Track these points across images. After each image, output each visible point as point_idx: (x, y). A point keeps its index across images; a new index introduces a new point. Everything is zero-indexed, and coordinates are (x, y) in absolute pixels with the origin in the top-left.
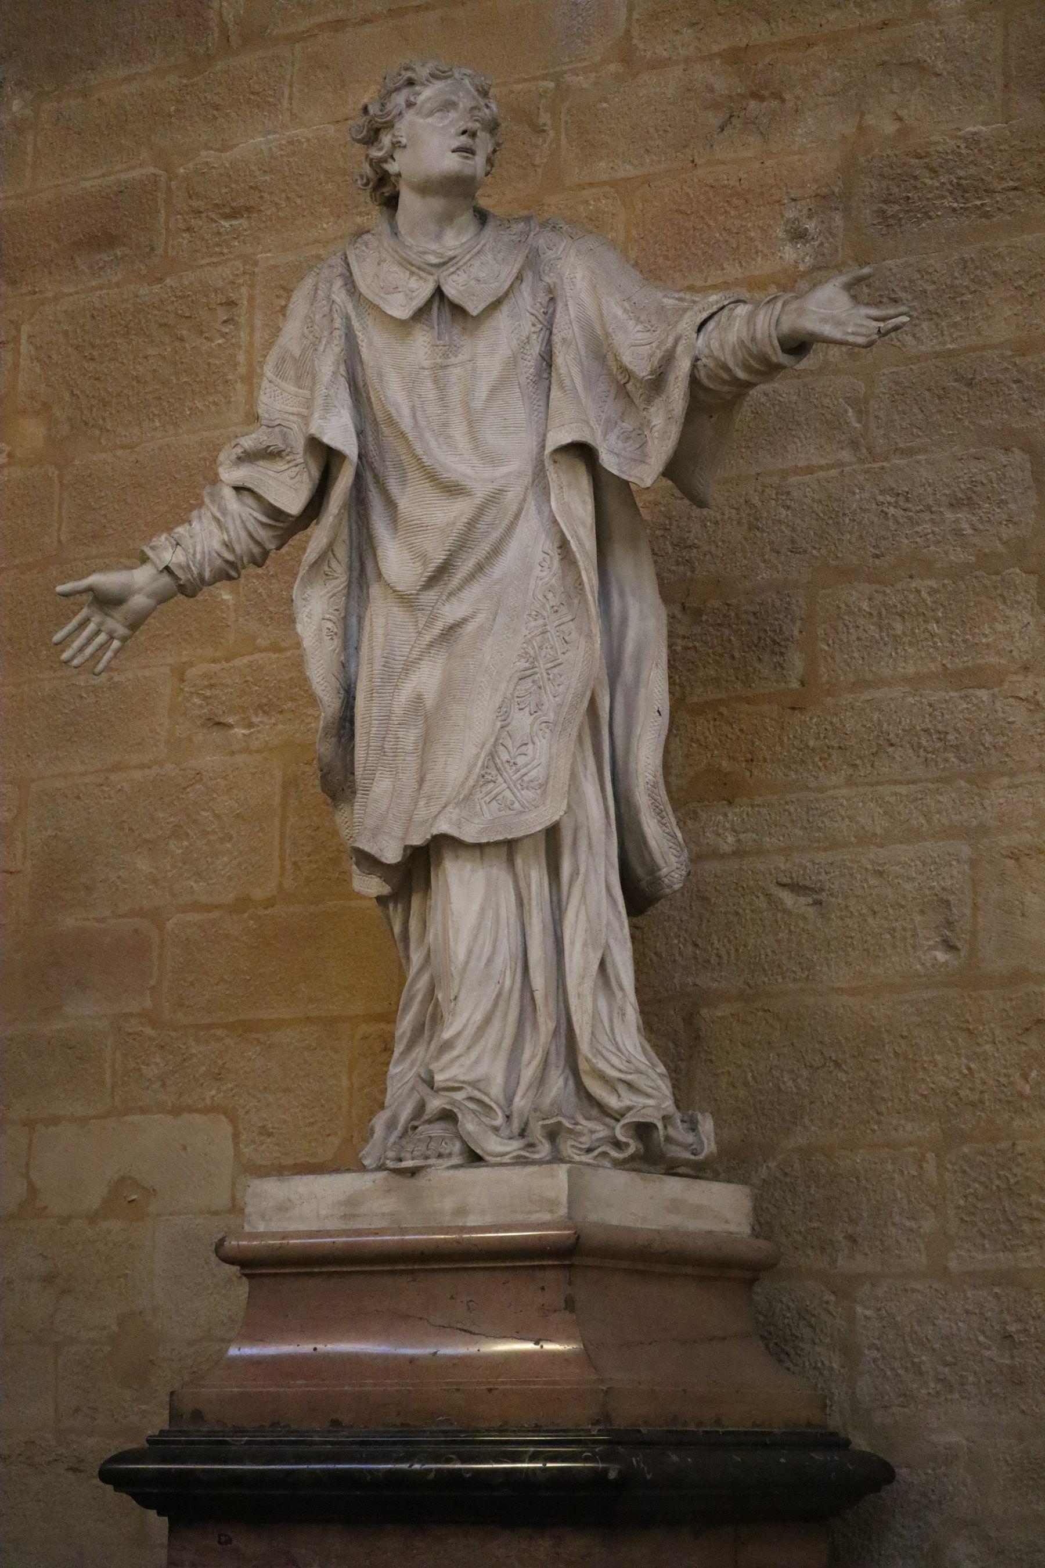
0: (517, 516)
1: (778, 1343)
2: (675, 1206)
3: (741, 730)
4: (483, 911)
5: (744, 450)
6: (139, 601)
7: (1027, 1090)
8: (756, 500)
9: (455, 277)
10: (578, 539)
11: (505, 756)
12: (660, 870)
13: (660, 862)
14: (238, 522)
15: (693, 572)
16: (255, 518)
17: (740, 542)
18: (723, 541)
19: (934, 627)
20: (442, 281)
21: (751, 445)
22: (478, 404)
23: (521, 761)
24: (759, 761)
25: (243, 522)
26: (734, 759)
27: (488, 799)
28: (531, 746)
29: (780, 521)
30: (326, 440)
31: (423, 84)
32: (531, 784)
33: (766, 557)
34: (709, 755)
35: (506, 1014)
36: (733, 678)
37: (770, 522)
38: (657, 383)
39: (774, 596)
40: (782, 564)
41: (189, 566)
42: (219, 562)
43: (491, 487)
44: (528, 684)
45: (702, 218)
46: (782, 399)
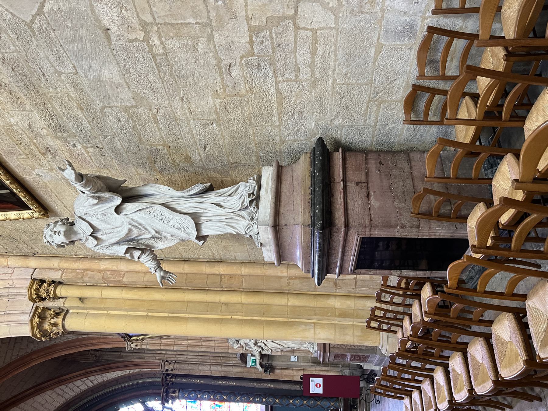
0: (132, 220)
1: (295, 157)
2: (266, 191)
4: (211, 229)
6: (162, 274)
7: (240, 111)
19: (147, 125)
23: (180, 222)
35: (230, 223)
38: (98, 198)
43: (128, 225)
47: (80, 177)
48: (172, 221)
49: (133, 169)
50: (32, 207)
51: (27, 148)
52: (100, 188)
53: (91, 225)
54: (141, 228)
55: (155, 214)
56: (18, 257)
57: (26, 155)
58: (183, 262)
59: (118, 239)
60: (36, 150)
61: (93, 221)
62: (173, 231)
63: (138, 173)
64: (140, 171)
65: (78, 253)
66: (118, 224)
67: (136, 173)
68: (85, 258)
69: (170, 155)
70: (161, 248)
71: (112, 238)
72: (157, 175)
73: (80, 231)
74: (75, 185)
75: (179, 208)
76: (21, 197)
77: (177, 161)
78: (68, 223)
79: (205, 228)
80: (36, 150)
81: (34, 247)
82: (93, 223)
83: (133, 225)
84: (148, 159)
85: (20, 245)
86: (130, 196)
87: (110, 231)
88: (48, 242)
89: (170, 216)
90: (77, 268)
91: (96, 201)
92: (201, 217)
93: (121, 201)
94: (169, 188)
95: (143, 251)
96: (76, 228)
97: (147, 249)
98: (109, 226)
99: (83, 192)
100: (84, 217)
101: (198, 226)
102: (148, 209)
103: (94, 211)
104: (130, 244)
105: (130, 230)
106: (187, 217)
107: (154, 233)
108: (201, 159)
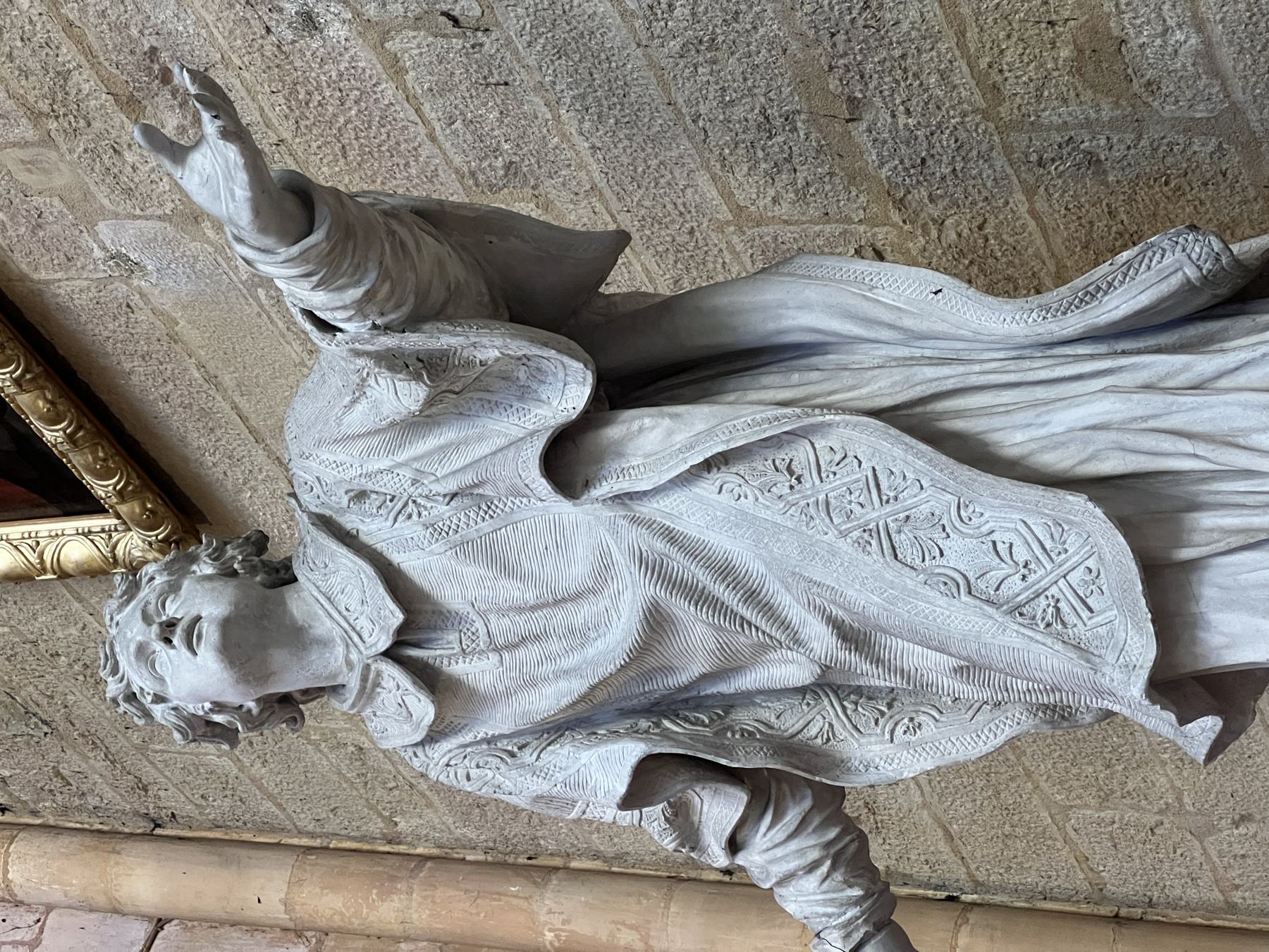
0: (671, 536)
3: (1009, 36)
5: (614, 65)
8: (675, 45)
9: (365, 636)
10: (690, 447)
11: (1015, 584)
12: (1188, 280)
13: (1175, 281)
14: (779, 852)
15: (799, 112)
16: (769, 828)
17: (739, 60)
18: (745, 80)
20: (373, 651)
21: (603, 56)
22: (530, 597)
23: (1021, 554)
24: (1048, 12)
25: (776, 846)
26: (1053, 43)
27: (1085, 614)
28: (995, 537)
29: (693, 14)
30: (622, 789)
31: (128, 685)
32: (1057, 536)
33: (749, 27)
34: (1056, 74)
36: (934, 53)
37: (697, 26)
39: (799, 14)
40: (751, 7)
41: (845, 925)
42: (838, 876)
44: (901, 540)
45: (340, 129)
46: (528, 25)
47: (292, 205)
48: (954, 546)
49: (702, 179)
50: (102, 488)
51: (33, 64)
52: (437, 295)
53: (394, 581)
54: (730, 598)
55: (832, 487)
56: (64, 840)
57: (36, 117)
58: (1108, 932)
59: (578, 686)
60: (84, 81)
61: (404, 547)
62: (965, 621)
63: (738, 210)
64: (747, 187)
65: (402, 826)
66: (577, 572)
67: (725, 214)
68: (444, 860)
69: (961, 33)
70: (889, 771)
71: (532, 683)
72: (871, 222)
73: (324, 626)
74: (267, 267)
75: (1013, 439)
76: (37, 425)
77: (1017, 85)
78: (253, 570)
79: (1229, 605)
80: (84, 81)
81: (148, 773)
82: (408, 562)
83: (688, 580)
84: (802, 83)
85: (72, 763)
86: (656, 360)
87: (523, 624)
88: (131, 697)
89: (942, 502)
90: (397, 929)
91: (407, 395)
92: (1196, 506)
93: (587, 391)
94: (940, 279)
95: (763, 792)
96: (303, 601)
97: (789, 781)
98: (511, 591)
99: (326, 327)
100: (350, 521)
101: (1167, 586)
102: (782, 456)
103: (408, 474)
104: (666, 735)
105: (656, 623)
106: (1077, 502)
107: (822, 640)
108: (1207, 54)
